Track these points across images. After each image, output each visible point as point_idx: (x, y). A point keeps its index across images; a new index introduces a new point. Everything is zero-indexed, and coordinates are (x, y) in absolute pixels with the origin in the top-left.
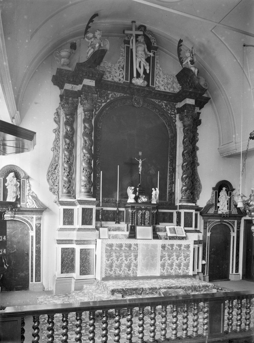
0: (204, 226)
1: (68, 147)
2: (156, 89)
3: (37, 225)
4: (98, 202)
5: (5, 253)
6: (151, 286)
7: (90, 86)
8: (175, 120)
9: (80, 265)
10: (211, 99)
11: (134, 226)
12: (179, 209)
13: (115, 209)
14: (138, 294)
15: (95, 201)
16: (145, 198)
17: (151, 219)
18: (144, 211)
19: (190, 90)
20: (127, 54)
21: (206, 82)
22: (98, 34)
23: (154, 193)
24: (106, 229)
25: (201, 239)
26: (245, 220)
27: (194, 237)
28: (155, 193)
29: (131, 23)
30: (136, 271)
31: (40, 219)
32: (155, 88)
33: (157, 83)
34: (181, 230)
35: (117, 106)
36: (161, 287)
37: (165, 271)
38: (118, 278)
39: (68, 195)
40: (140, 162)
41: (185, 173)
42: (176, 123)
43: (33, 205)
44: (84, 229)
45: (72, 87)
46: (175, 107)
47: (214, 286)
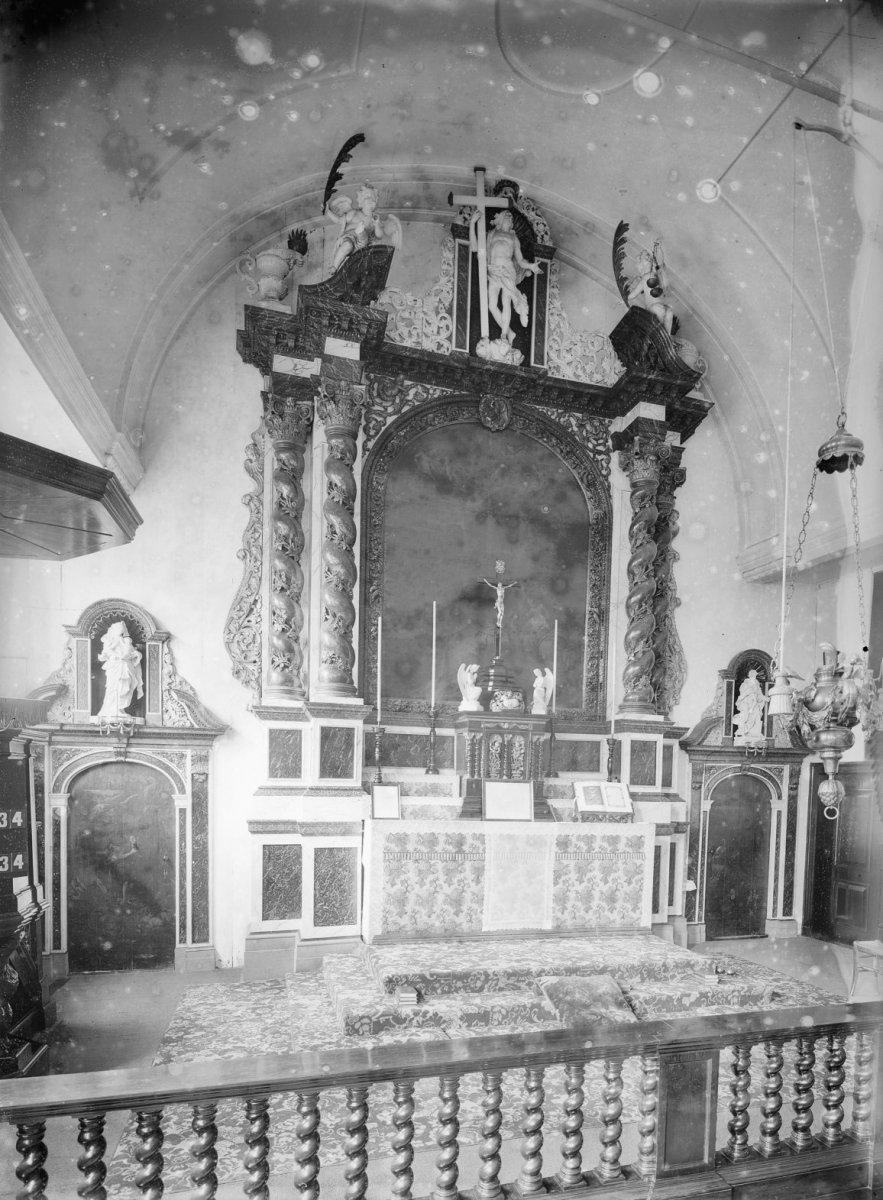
0: (790, 783)
1: (283, 547)
2: (550, 375)
3: (196, 777)
4: (369, 709)
5: (20, 867)
6: (515, 964)
8: (608, 468)
9: (315, 895)
10: (716, 406)
11: (476, 780)
12: (617, 731)
13: (425, 731)
14: (473, 991)
15: (360, 707)
16: (511, 698)
17: (528, 761)
18: (508, 737)
19: (650, 377)
20: (462, 268)
21: (701, 358)
22: (367, 199)
23: (538, 683)
24: (393, 791)
25: (682, 819)
26: (812, 765)
27: (661, 812)
28: (545, 682)
29: (473, 174)
30: (479, 914)
31: (204, 759)
33: (553, 355)
34: (616, 795)
35: (431, 425)
36: (546, 968)
37: (567, 916)
38: (423, 936)
39: (286, 688)
40: (500, 592)
41: (634, 624)
42: (611, 479)
43: (185, 718)
44: (328, 789)
45: (296, 365)
46: (607, 432)
47: (710, 965)
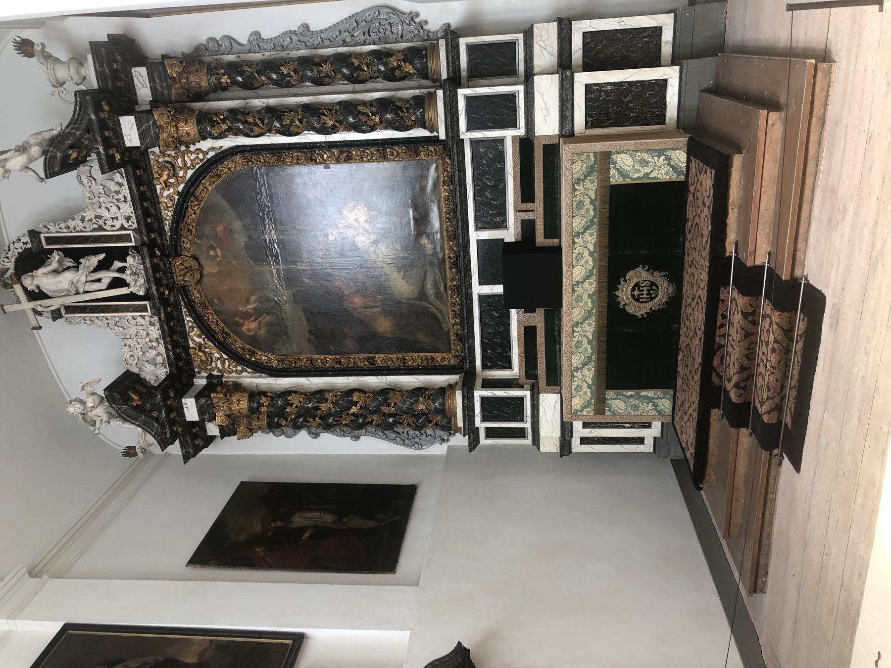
2: (135, 226)
7: (198, 411)
32: (134, 230)
